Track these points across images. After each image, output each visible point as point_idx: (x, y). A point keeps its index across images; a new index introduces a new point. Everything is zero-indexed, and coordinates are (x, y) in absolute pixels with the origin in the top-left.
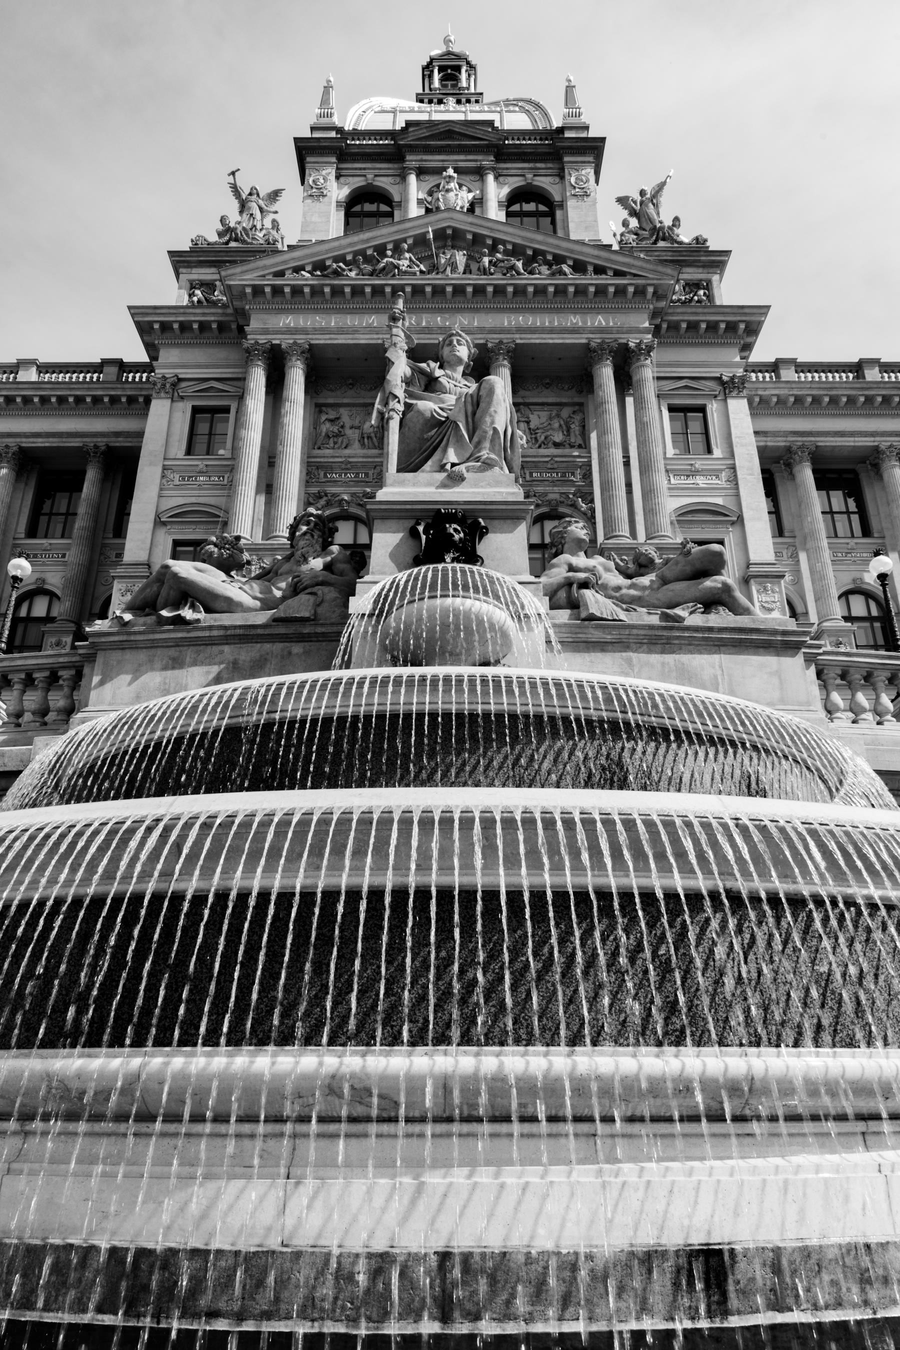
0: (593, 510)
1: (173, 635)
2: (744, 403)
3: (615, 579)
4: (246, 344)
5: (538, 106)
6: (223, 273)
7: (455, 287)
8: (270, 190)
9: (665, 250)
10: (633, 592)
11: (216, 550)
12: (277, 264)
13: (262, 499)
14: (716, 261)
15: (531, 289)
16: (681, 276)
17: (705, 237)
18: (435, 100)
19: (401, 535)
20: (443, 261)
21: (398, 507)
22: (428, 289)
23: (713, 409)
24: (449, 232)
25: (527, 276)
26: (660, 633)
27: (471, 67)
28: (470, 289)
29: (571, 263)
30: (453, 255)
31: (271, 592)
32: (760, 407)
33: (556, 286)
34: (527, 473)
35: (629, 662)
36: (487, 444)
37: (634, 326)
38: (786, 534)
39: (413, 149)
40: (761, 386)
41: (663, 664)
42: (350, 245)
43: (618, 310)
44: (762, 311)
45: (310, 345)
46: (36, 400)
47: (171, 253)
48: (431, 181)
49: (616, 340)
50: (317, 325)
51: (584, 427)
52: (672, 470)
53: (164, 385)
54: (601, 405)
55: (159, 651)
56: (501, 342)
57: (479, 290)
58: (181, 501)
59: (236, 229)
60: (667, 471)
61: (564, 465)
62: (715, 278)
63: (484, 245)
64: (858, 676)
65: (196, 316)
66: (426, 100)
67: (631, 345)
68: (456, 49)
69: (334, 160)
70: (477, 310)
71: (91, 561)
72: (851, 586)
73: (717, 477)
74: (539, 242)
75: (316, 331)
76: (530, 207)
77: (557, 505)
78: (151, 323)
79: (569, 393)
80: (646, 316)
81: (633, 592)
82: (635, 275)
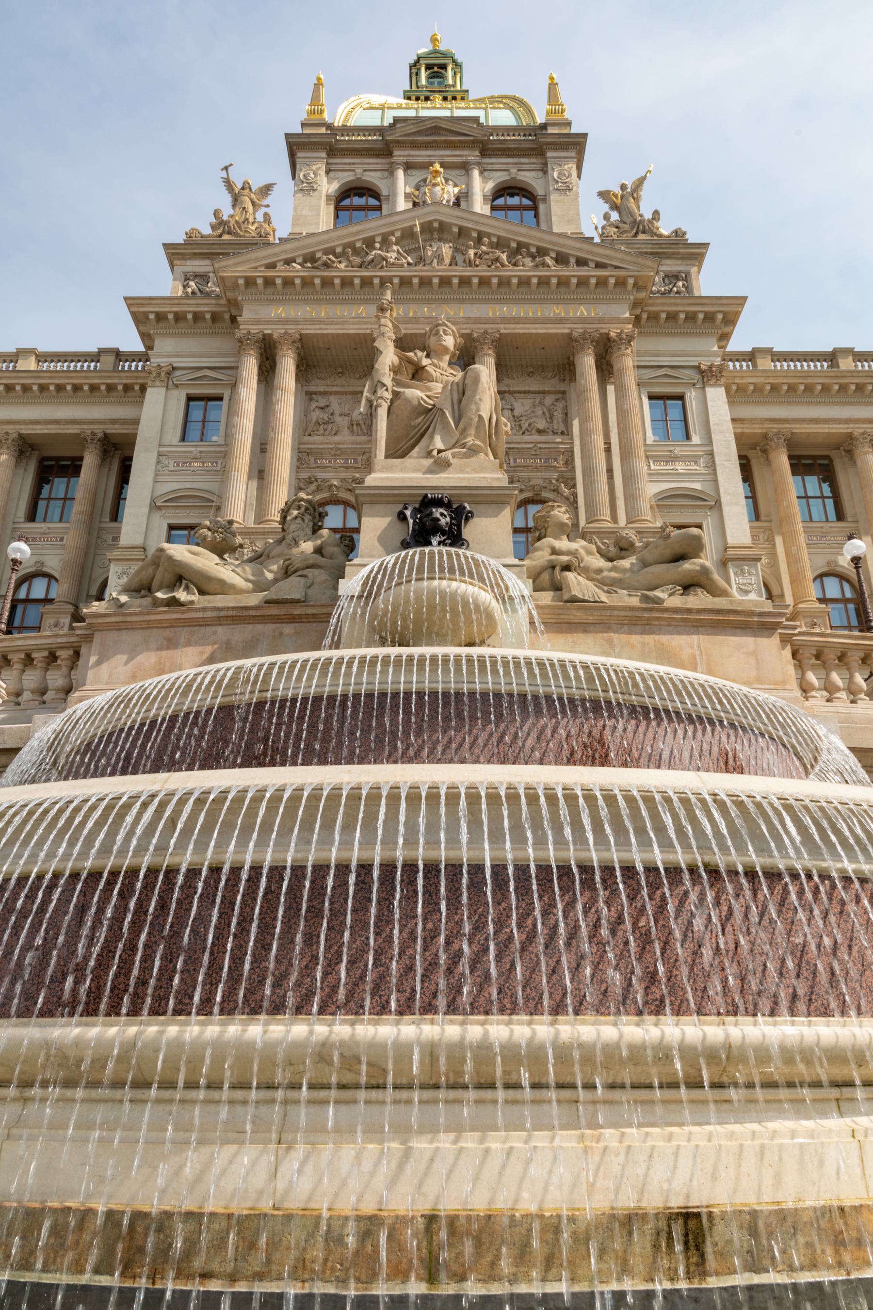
0: (575, 495)
1: (167, 616)
2: (722, 391)
3: (597, 562)
4: (239, 334)
5: (522, 103)
9: (646, 243)
10: (613, 574)
11: (210, 533)
12: (269, 256)
13: (254, 484)
14: (696, 253)
15: (515, 281)
16: (661, 268)
17: (684, 229)
18: (422, 98)
19: (389, 519)
20: (430, 253)
22: (416, 281)
23: (692, 397)
24: (436, 225)
25: (511, 268)
26: (640, 614)
27: (457, 65)
28: (455, 281)
29: (554, 255)
30: (439, 248)
31: (263, 574)
32: (737, 395)
33: (540, 277)
34: (512, 458)
35: (610, 642)
36: (472, 431)
37: (615, 316)
38: (763, 518)
39: (400, 144)
40: (738, 374)
41: (643, 644)
42: (339, 238)
44: (740, 302)
45: (301, 335)
46: (35, 388)
47: (166, 246)
48: (418, 175)
49: (597, 330)
50: (308, 316)
52: (652, 456)
53: (159, 374)
54: (583, 393)
55: (154, 631)
56: (486, 332)
57: (465, 282)
58: (176, 486)
59: (229, 222)
60: (647, 457)
61: (548, 451)
62: (694, 270)
63: (469, 237)
65: (190, 307)
66: (413, 98)
67: (613, 334)
68: (442, 47)
69: (324, 155)
70: (463, 301)
71: (88, 545)
73: (696, 463)
74: (522, 235)
76: (515, 201)
78: (146, 314)
79: (553, 381)
80: (626, 307)
81: (613, 574)
82: (616, 267)
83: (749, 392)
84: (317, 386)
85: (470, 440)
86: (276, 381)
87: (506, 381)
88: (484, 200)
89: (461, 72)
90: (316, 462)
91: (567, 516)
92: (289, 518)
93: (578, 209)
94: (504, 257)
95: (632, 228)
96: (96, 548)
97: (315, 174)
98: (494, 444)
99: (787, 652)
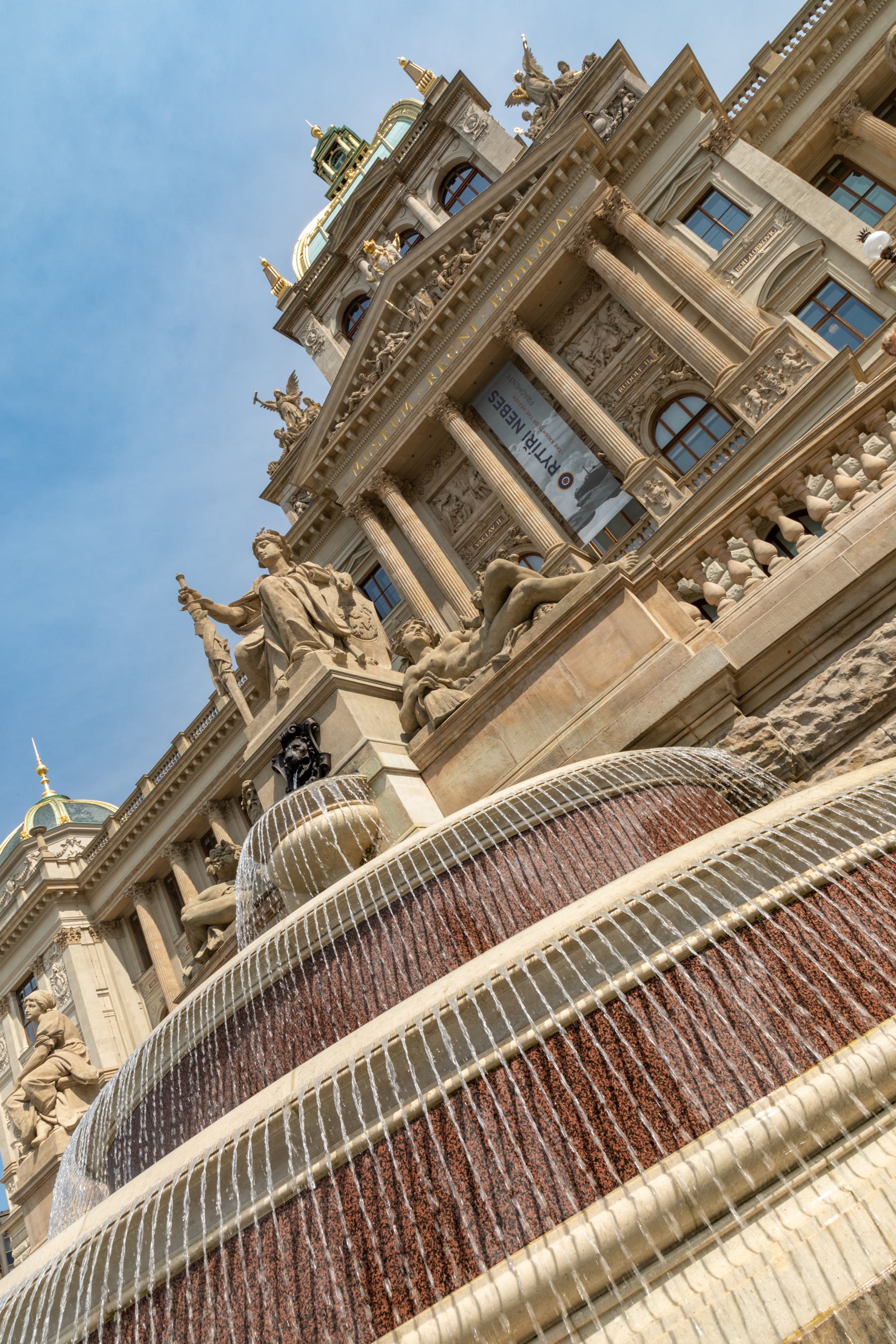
4: (346, 513)
5: (401, 106)
6: (293, 482)
12: (318, 439)
14: (618, 59)
15: (488, 262)
20: (413, 314)
22: (422, 345)
23: (720, 179)
24: (401, 287)
25: (477, 255)
26: (498, 686)
27: (343, 132)
29: (499, 208)
30: (416, 302)
32: (757, 135)
33: (504, 237)
36: (293, 638)
39: (346, 245)
41: (520, 710)
43: (566, 199)
45: (384, 469)
47: (262, 496)
49: (584, 224)
50: (377, 450)
51: (626, 311)
52: (729, 267)
57: (455, 305)
62: (627, 76)
63: (431, 268)
68: (324, 132)
69: (308, 312)
70: (468, 319)
73: (774, 229)
74: (464, 221)
75: (380, 455)
77: (658, 395)
82: (553, 160)
83: (780, 105)
84: (430, 489)
90: (475, 548)
94: (466, 254)
97: (314, 332)
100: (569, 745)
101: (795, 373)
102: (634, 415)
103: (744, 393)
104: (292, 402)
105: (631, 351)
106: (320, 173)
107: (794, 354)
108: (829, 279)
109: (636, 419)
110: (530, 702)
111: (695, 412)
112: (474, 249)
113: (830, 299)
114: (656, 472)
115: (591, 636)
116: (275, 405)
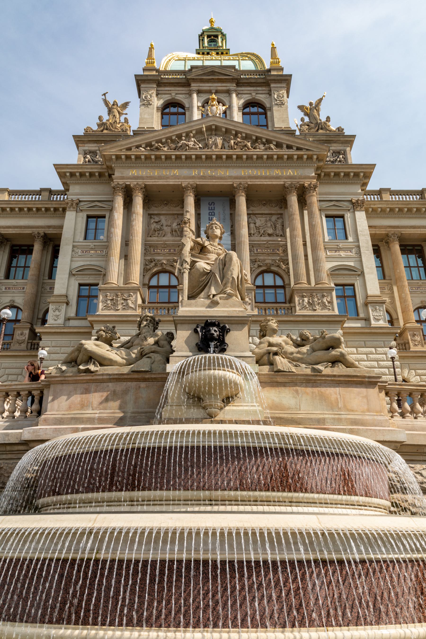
0: (288, 269)
1: (85, 378)
2: (363, 213)
3: (291, 349)
5: (257, 57)
7: (217, 155)
8: (123, 102)
9: (323, 135)
10: (299, 355)
11: (104, 334)
13: (123, 261)
14: (349, 140)
15: (255, 157)
16: (331, 148)
17: (342, 127)
18: (206, 53)
19: (190, 332)
20: (211, 142)
21: (188, 319)
22: (204, 157)
23: (348, 216)
24: (214, 127)
25: (253, 150)
27: (224, 35)
28: (224, 157)
29: (275, 143)
30: (216, 139)
31: (130, 355)
32: (372, 213)
33: (268, 155)
35: (297, 391)
37: (307, 174)
38: (387, 278)
39: (194, 80)
40: (373, 203)
41: (313, 393)
42: (164, 134)
43: (299, 167)
44: (372, 167)
45: (145, 185)
46: (8, 209)
48: (204, 97)
50: (148, 175)
51: (283, 226)
52: (328, 248)
53: (72, 204)
54: (291, 216)
55: (79, 385)
57: (229, 157)
58: (82, 263)
59: (107, 123)
61: (274, 245)
62: (348, 149)
64: (405, 395)
65: (87, 170)
66: (201, 53)
67: (306, 185)
68: (215, 26)
69: (155, 86)
70: (228, 167)
71: (37, 291)
72: (420, 305)
73: (351, 251)
74: (258, 133)
76: (254, 110)
78: (65, 173)
79: (276, 208)
80: (313, 170)
81: (299, 355)
82: (307, 150)
83: (379, 212)
85: (229, 290)
86: (133, 209)
87: (252, 208)
88: (239, 109)
89: (226, 39)
90: (154, 251)
91: (276, 325)
92: (142, 326)
93: (287, 115)
94: (249, 144)
95: (316, 127)
96: (41, 293)
97: (151, 96)
98: (240, 289)
99: (383, 394)
100: (328, 421)
101: (324, 307)
102: (256, 263)
103: (303, 297)
104: (119, 112)
105: (274, 241)
106: (201, 38)
107: (329, 300)
108: (353, 285)
109: (256, 266)
110: (318, 393)
111: (277, 284)
112: (254, 146)
113: (349, 292)
114: (252, 293)
115: (356, 390)
116: (110, 106)
